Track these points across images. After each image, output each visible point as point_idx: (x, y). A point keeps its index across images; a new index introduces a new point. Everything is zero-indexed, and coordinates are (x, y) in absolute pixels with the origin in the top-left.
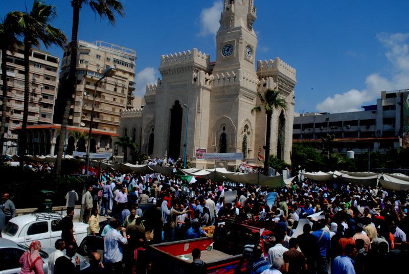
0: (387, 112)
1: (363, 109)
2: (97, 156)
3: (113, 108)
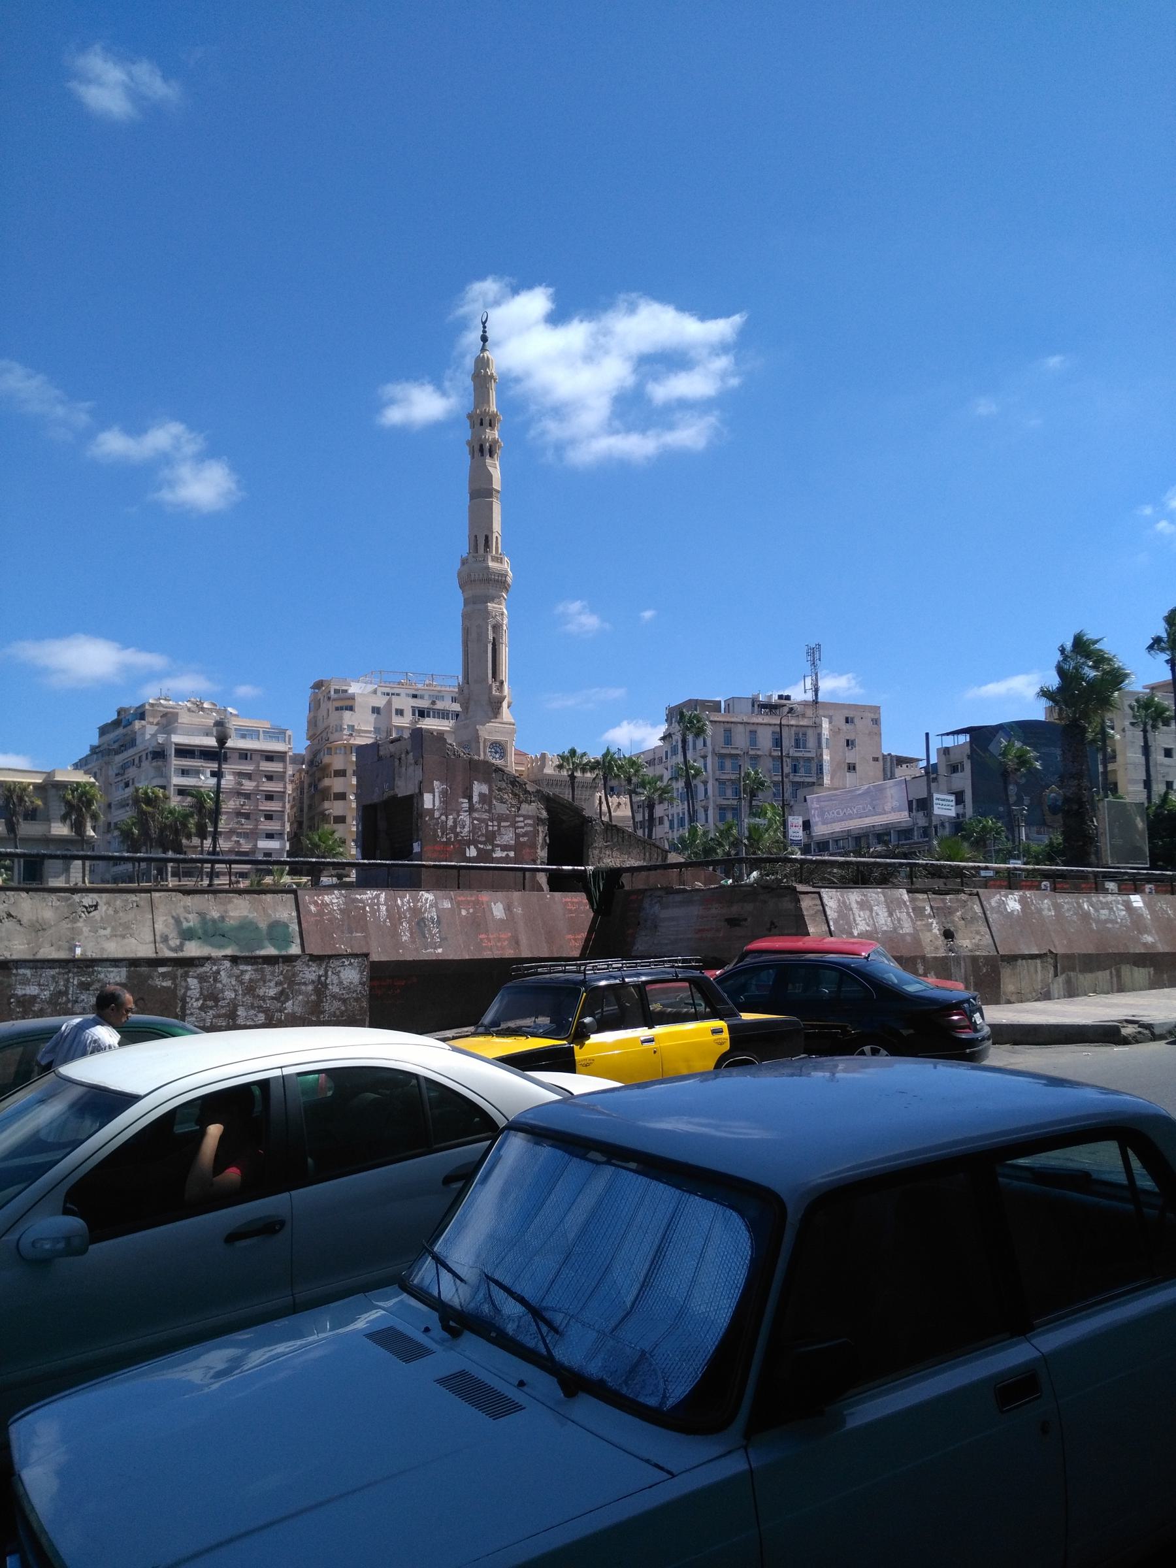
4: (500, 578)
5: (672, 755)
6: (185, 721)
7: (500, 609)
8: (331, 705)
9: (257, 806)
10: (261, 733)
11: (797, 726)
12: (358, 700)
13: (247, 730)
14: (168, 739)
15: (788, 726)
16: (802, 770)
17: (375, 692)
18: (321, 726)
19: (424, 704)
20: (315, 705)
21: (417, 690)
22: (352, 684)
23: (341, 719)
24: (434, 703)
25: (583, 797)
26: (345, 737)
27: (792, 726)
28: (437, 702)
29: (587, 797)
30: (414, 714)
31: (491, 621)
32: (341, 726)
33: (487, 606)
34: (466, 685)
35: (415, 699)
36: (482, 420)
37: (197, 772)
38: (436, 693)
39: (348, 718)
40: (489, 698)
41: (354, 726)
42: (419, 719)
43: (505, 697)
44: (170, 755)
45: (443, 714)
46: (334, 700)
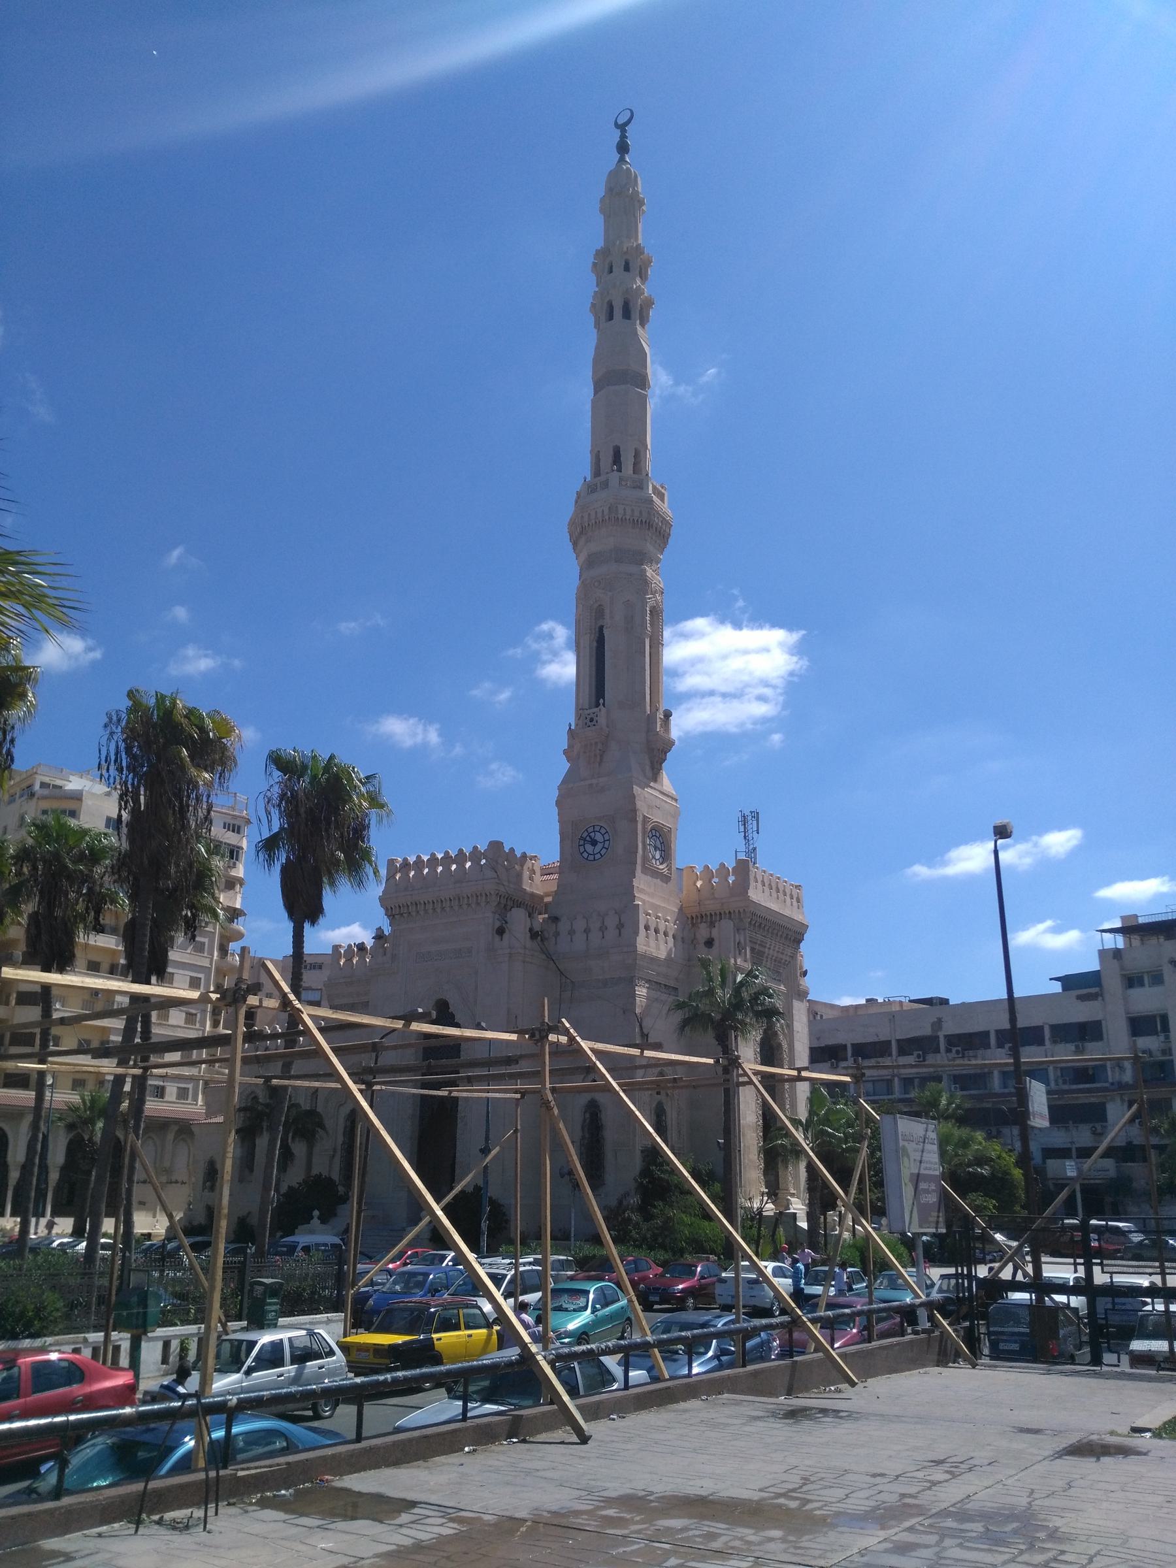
0: (1135, 992)
1: (1057, 987)
2: (1086, 1060)
3: (188, 1014)
12: (87, 802)
22: (72, 778)
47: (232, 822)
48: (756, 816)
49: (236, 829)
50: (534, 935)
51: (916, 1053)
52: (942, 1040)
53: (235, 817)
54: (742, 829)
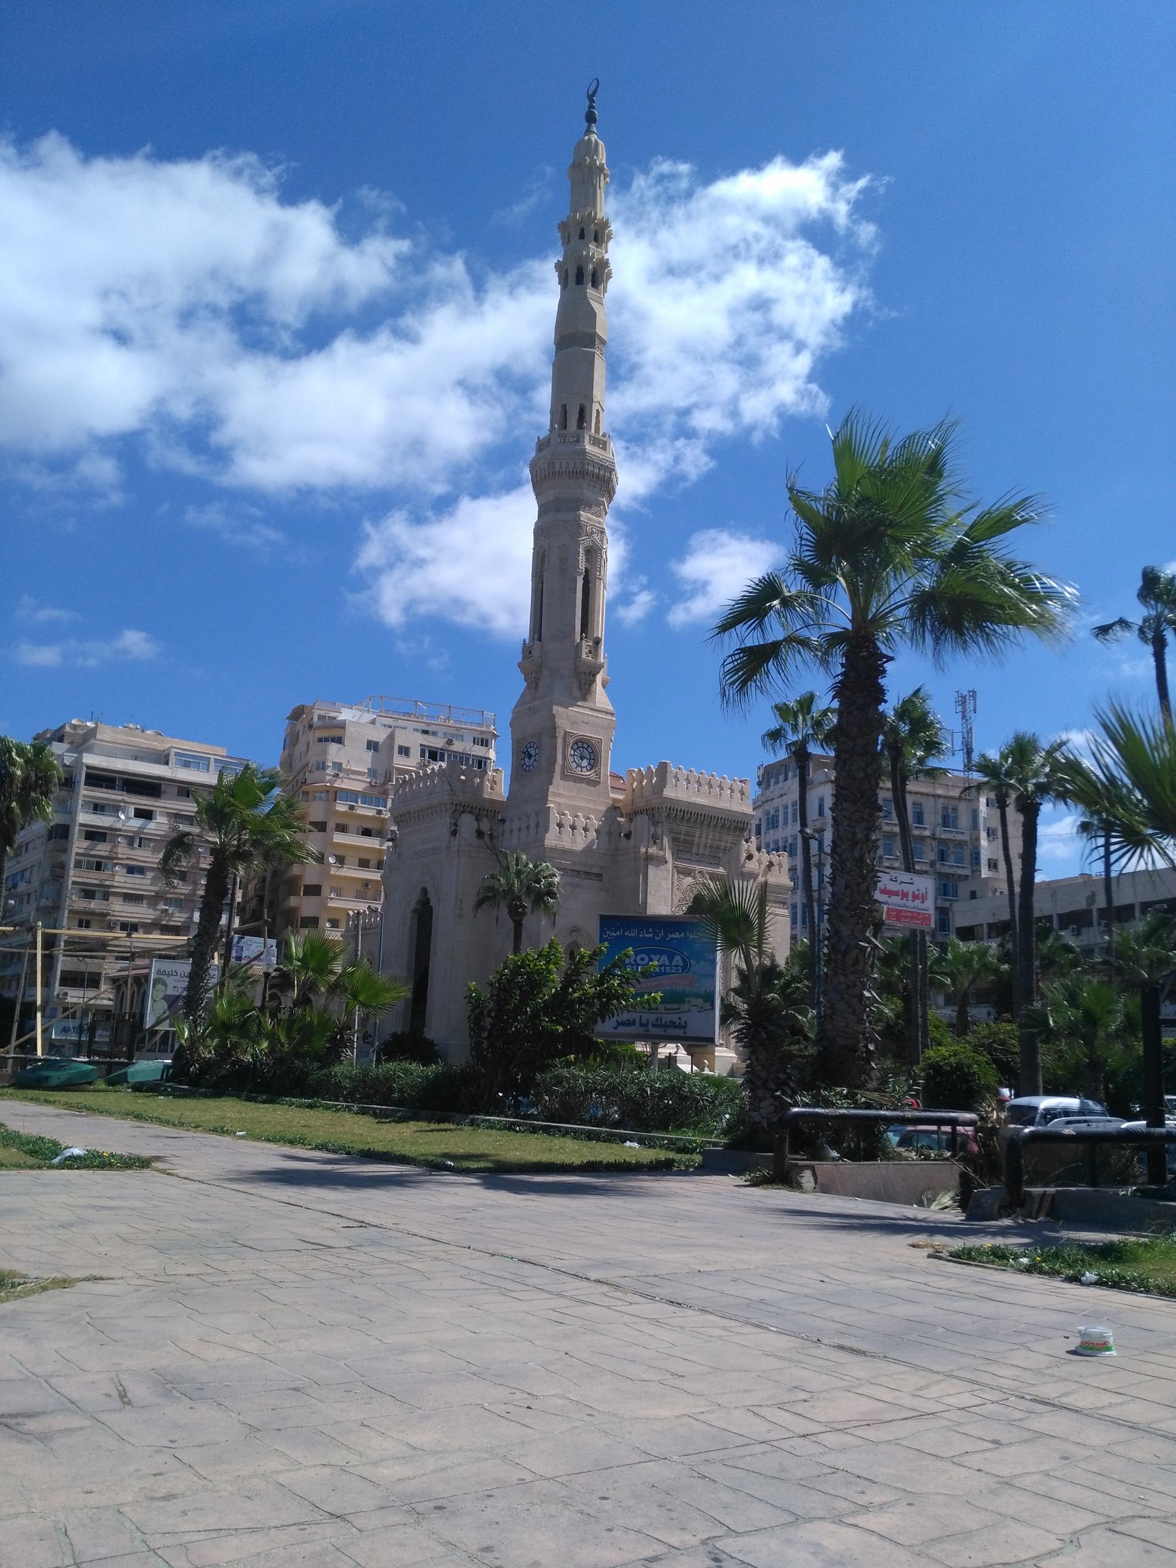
4: (602, 473)
5: (768, 829)
6: (106, 737)
7: (600, 523)
8: (312, 736)
9: (198, 863)
10: (212, 762)
11: (945, 797)
12: (350, 729)
13: (193, 756)
14: (78, 760)
15: (934, 796)
16: (952, 858)
17: (373, 722)
18: (297, 766)
19: (438, 743)
20: (292, 740)
21: (429, 724)
22: (343, 710)
23: (325, 752)
24: (450, 742)
25: (723, 844)
26: (328, 778)
27: (939, 796)
28: (455, 742)
29: (729, 845)
30: (423, 755)
31: (584, 542)
32: (324, 763)
33: (579, 516)
34: (537, 643)
35: (425, 736)
36: (582, 231)
37: (115, 809)
38: (452, 731)
39: (334, 752)
40: (576, 666)
41: (341, 764)
42: (429, 762)
43: (601, 666)
44: (79, 782)
45: (461, 758)
46: (318, 728)
47: (481, 736)
48: (973, 694)
49: (485, 743)
50: (480, 834)
51: (1071, 927)
52: (1095, 914)
53: (482, 732)
54: (960, 709)
